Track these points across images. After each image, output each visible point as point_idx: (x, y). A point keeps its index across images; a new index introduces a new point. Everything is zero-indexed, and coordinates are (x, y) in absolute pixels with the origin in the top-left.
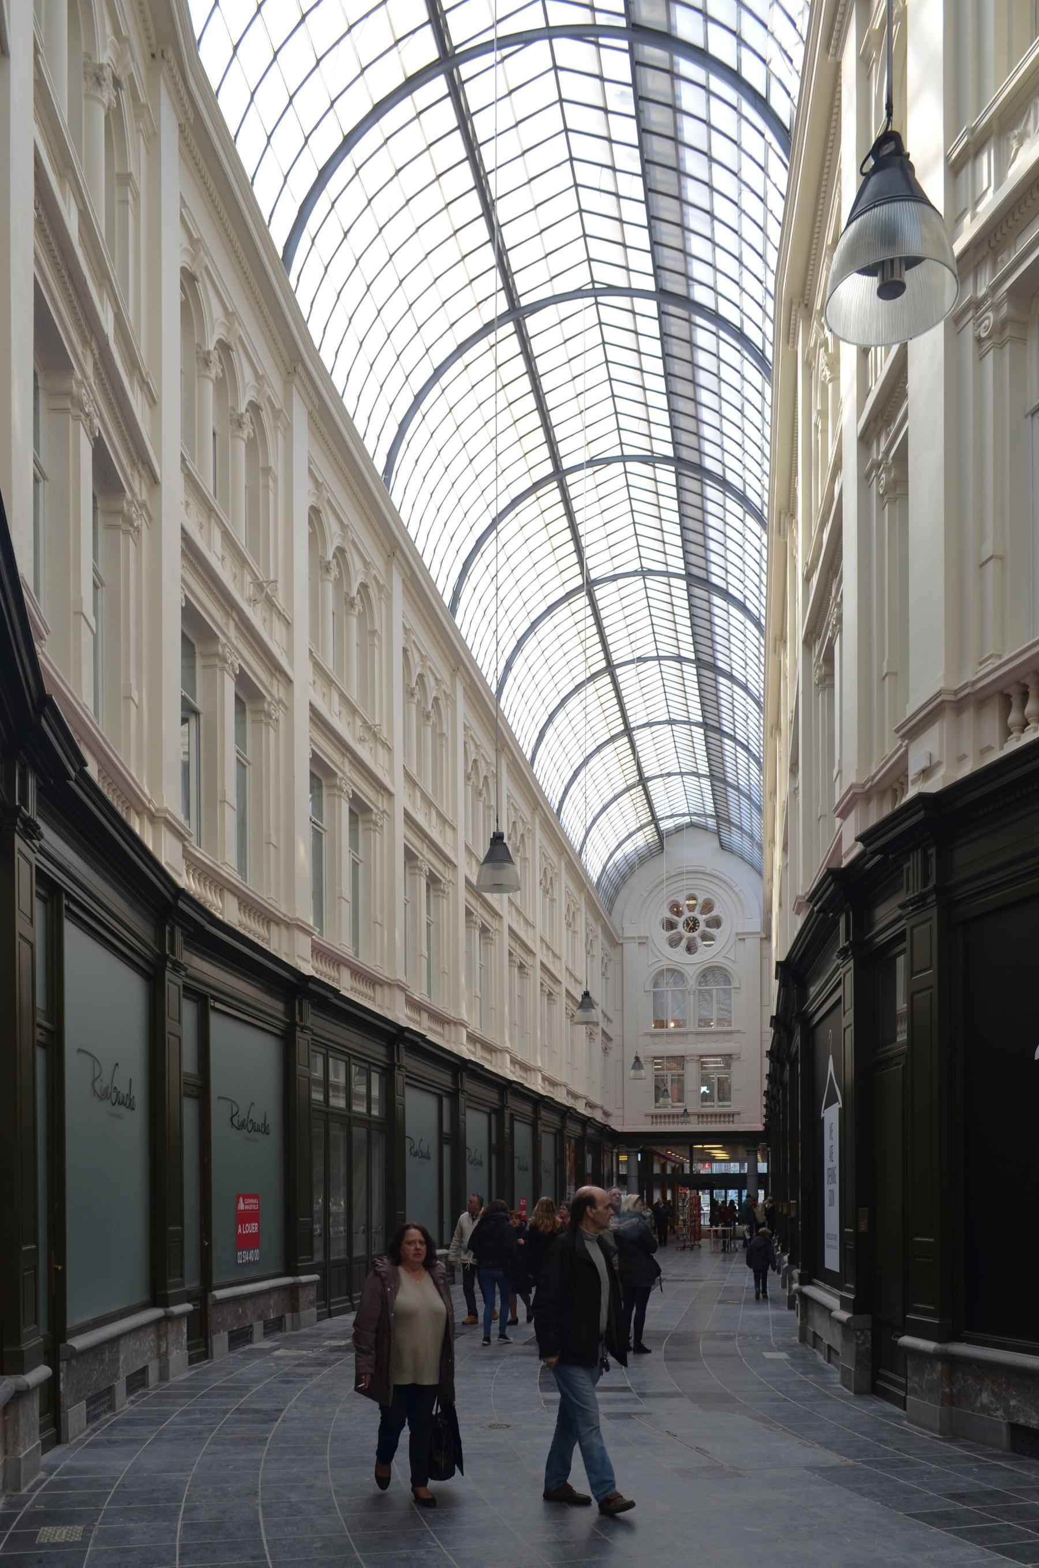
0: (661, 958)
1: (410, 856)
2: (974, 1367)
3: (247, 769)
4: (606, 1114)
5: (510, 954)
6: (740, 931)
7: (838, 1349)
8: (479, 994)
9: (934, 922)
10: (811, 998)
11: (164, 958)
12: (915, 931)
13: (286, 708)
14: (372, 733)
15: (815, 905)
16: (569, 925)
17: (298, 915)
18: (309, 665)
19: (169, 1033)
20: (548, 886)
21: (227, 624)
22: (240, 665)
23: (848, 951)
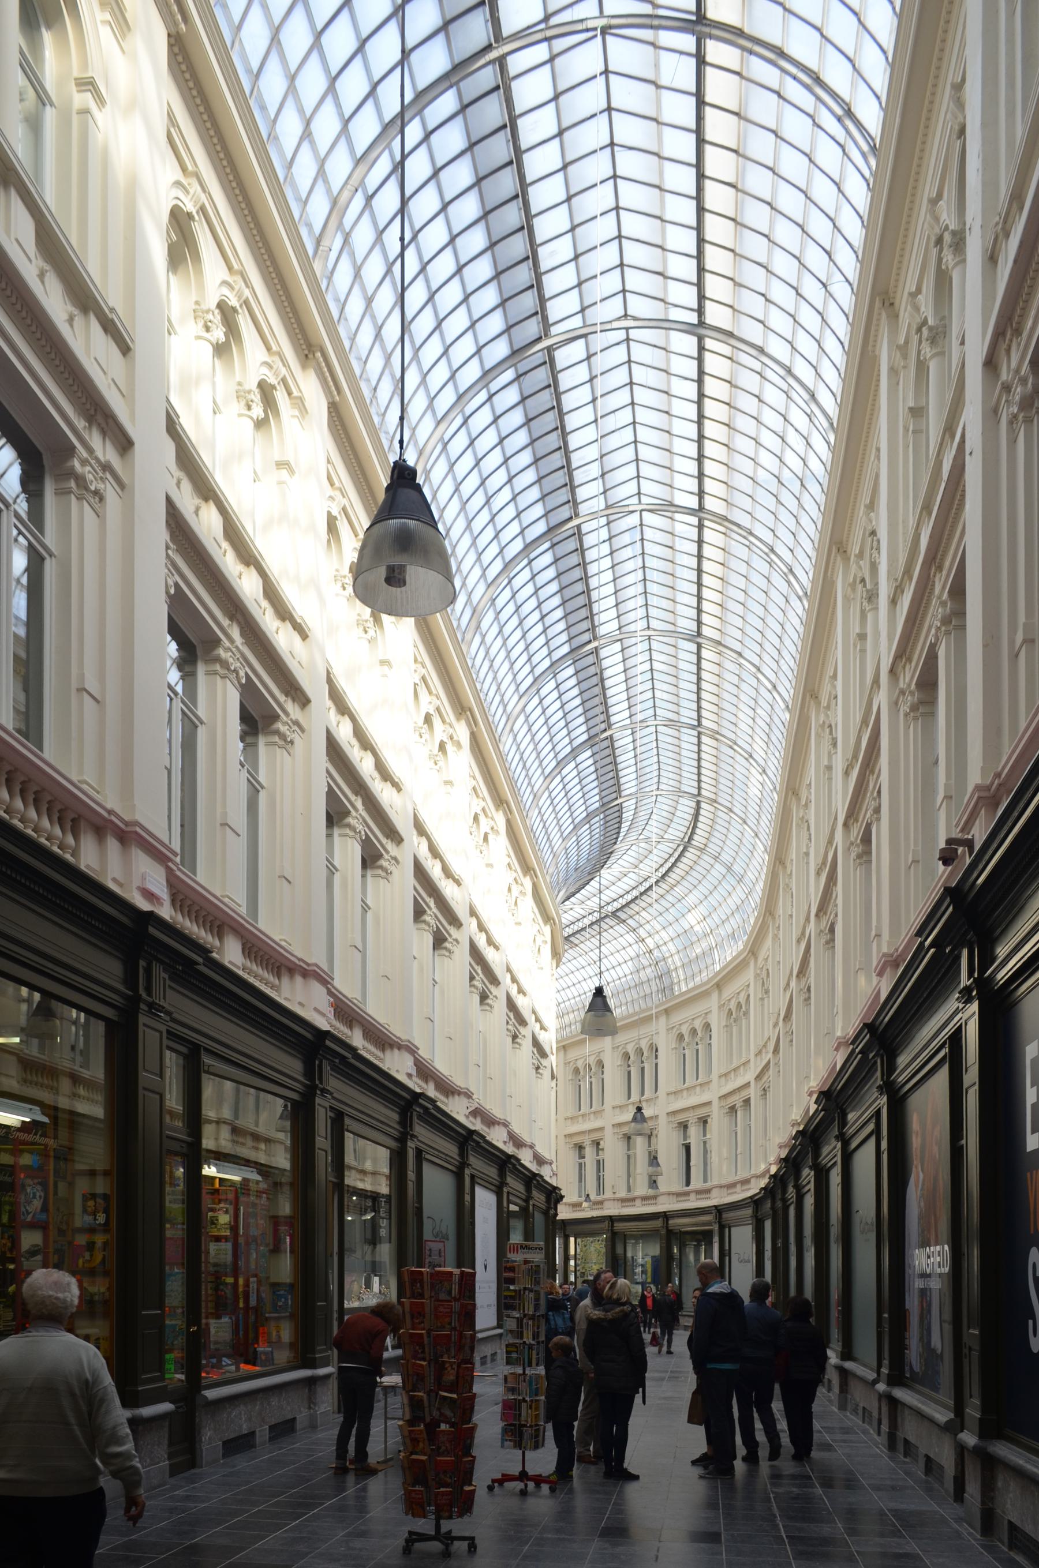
3: (261, 794)
11: (136, 1000)
17: (139, 817)
18: (169, 448)
19: (145, 1089)
23: (972, 991)
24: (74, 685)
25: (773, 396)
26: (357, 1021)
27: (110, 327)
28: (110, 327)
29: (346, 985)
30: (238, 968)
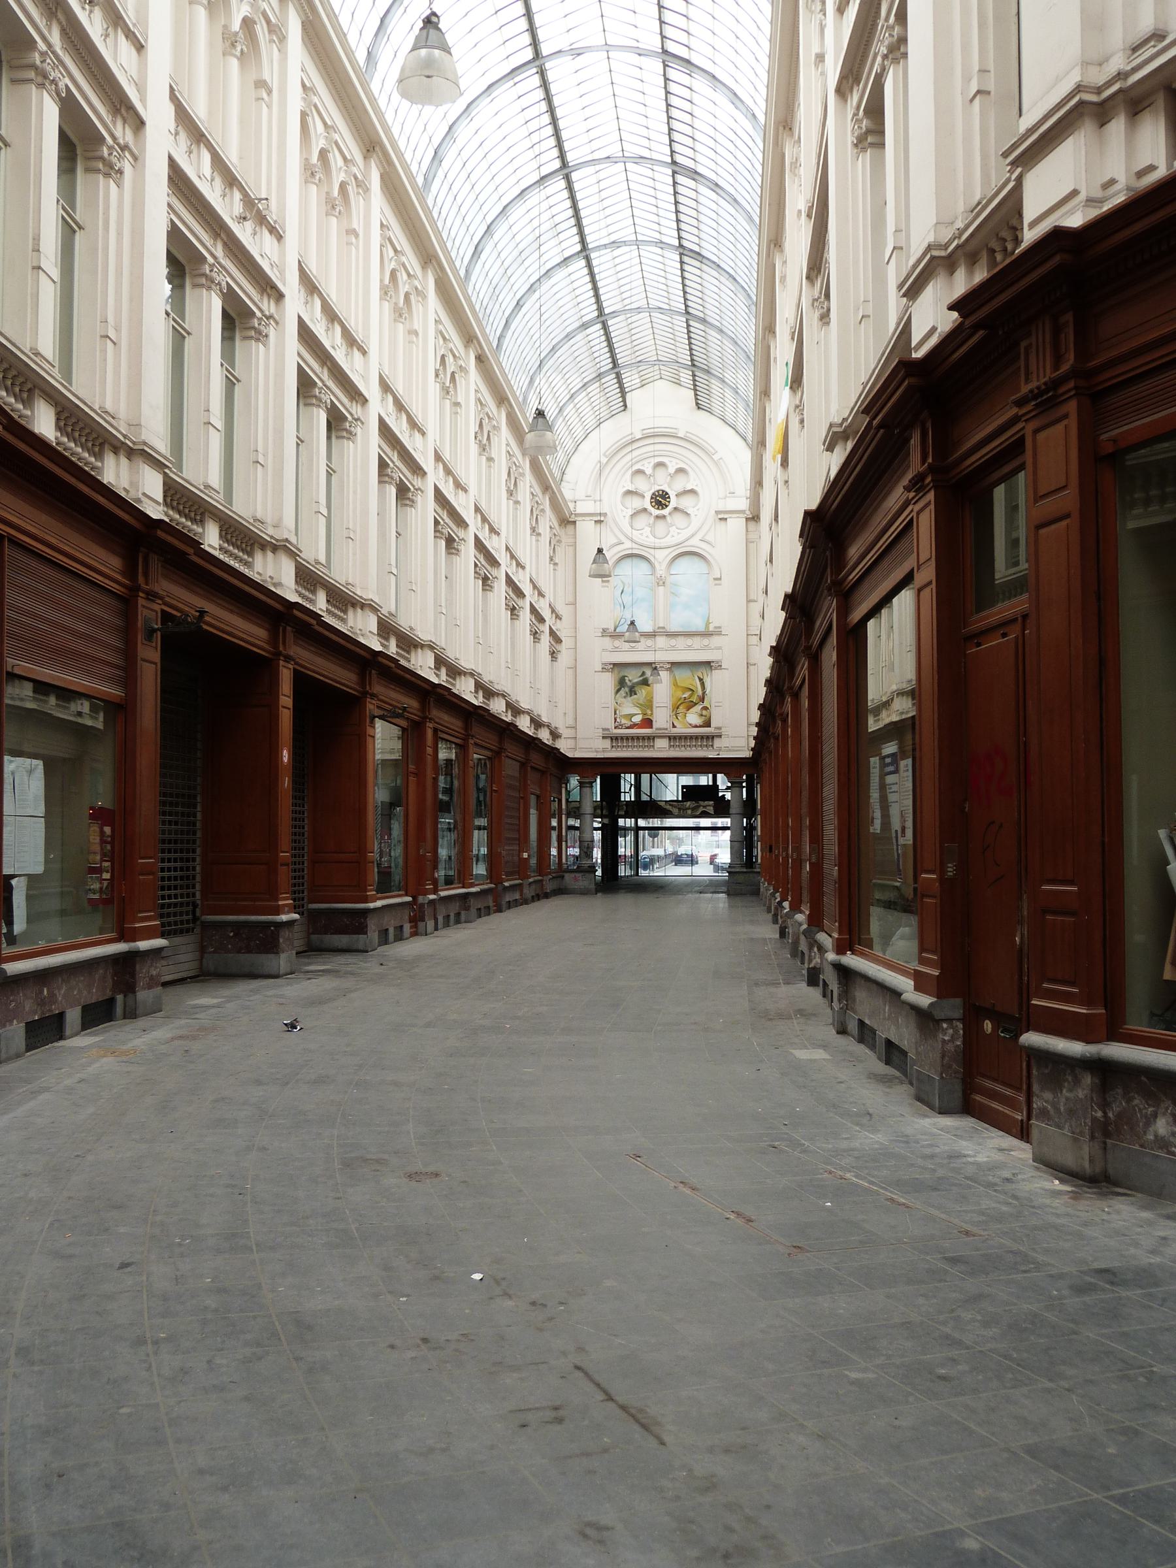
0: (623, 539)
2: (1143, 1078)
4: (555, 735)
5: (436, 522)
6: (721, 508)
7: (905, 1044)
9: (1073, 422)
10: (851, 563)
12: (1041, 436)
13: (135, 158)
14: (255, 212)
15: (874, 418)
16: (510, 493)
18: (170, 109)
20: (485, 441)
22: (67, 86)
26: (210, 512)
27: (130, 35)
28: (130, 35)
29: (313, 551)
30: (215, 549)
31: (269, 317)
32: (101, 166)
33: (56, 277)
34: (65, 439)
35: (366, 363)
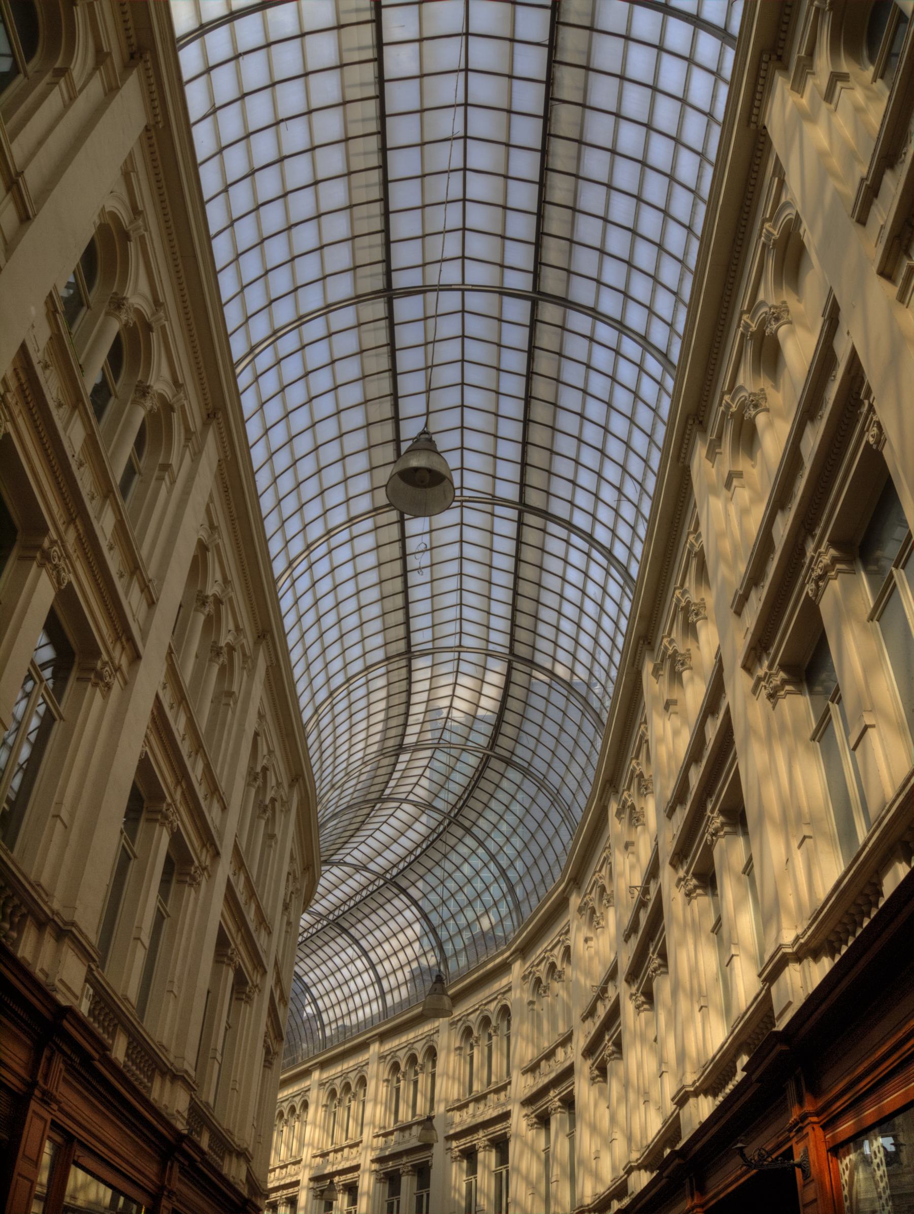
1: (222, 942)
8: (219, 1057)
11: (33, 1085)
19: (19, 1175)
21: (201, 852)
24: (52, 811)
25: (576, 557)
28: (221, 800)
31: (205, 869)
32: (225, 960)
33: (147, 945)
34: (130, 1063)
35: (270, 942)
